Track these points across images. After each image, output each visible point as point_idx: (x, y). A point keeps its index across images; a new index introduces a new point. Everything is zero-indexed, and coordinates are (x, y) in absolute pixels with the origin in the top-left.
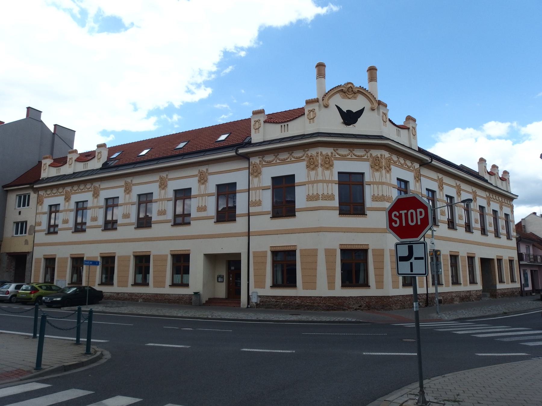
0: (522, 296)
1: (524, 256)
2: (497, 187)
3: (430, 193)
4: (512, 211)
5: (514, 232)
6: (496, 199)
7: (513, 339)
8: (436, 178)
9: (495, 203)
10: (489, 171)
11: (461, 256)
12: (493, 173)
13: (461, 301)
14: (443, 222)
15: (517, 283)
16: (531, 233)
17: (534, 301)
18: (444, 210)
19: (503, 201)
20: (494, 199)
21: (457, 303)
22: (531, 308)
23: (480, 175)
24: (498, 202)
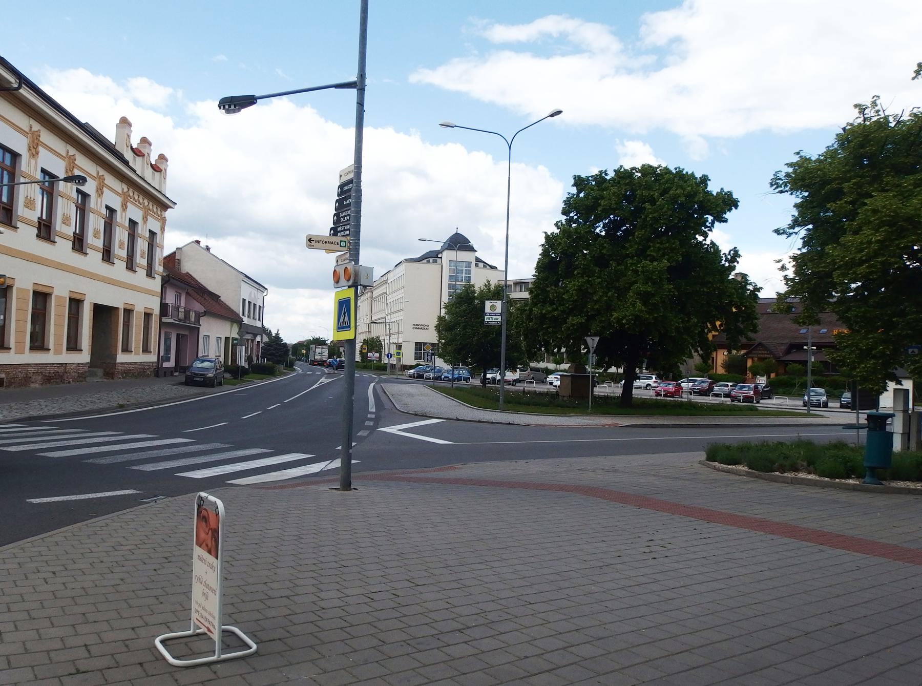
0: (158, 377)
1: (171, 308)
2: (143, 179)
3: (8, 156)
4: (163, 229)
5: (160, 265)
6: (139, 201)
7: (120, 459)
8: (27, 129)
9: (134, 207)
10: (133, 147)
11: (136, 312)
12: (140, 151)
13: (46, 384)
14: (28, 222)
15: (152, 353)
16: (188, 273)
17: (174, 385)
18: (32, 199)
19: (151, 207)
20: (153, 212)
21: (37, 385)
22: (167, 397)
23: (116, 148)
24: (160, 218)
